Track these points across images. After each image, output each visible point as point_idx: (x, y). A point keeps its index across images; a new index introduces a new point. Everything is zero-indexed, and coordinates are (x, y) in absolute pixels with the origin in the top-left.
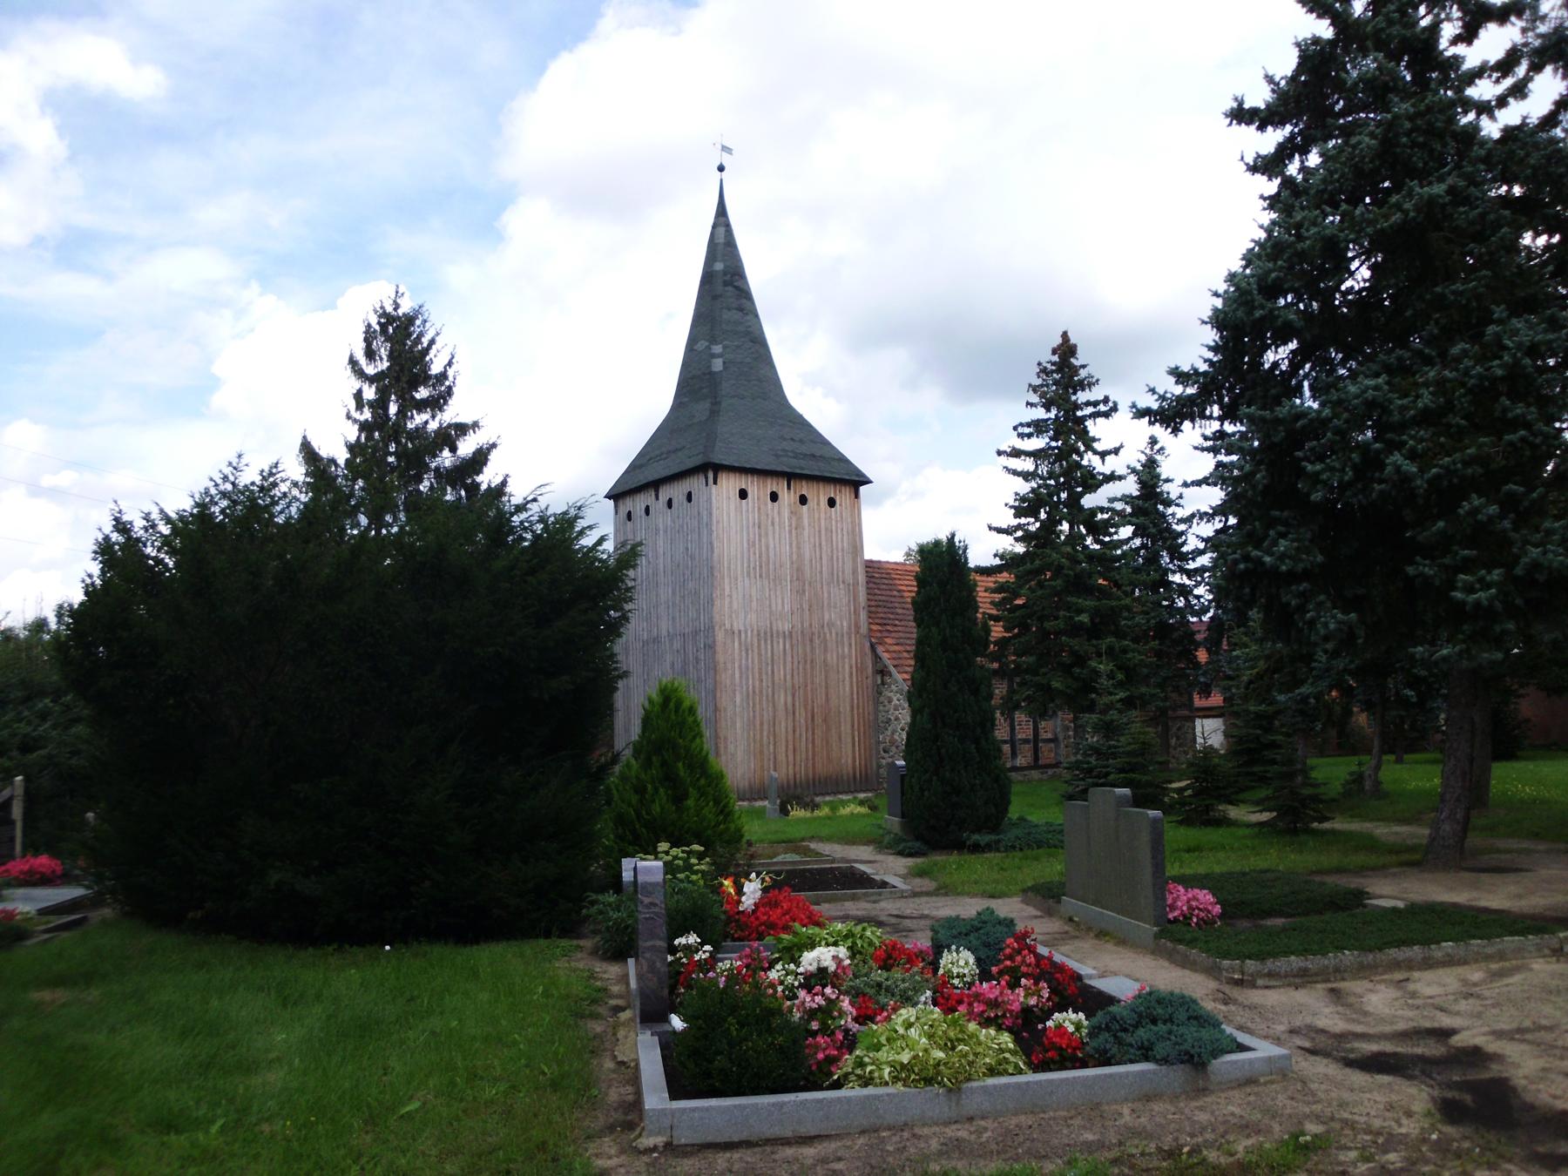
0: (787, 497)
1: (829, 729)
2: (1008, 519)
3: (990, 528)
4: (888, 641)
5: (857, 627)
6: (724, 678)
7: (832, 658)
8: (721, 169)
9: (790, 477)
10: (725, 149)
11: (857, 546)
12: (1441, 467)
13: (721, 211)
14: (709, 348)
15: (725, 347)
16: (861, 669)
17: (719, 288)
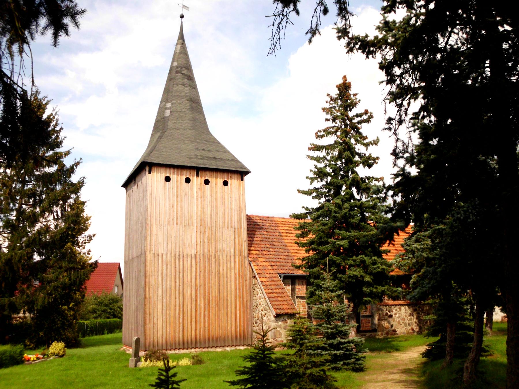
0: (197, 181)
1: (219, 310)
2: (307, 186)
3: (299, 191)
4: (260, 260)
5: (240, 252)
6: (152, 280)
7: (223, 269)
8: (182, 17)
9: (199, 170)
10: (184, 6)
11: (241, 208)
12: (413, 59)
13: (181, 37)
14: (165, 105)
15: (172, 104)
16: (242, 276)
17: (174, 74)
